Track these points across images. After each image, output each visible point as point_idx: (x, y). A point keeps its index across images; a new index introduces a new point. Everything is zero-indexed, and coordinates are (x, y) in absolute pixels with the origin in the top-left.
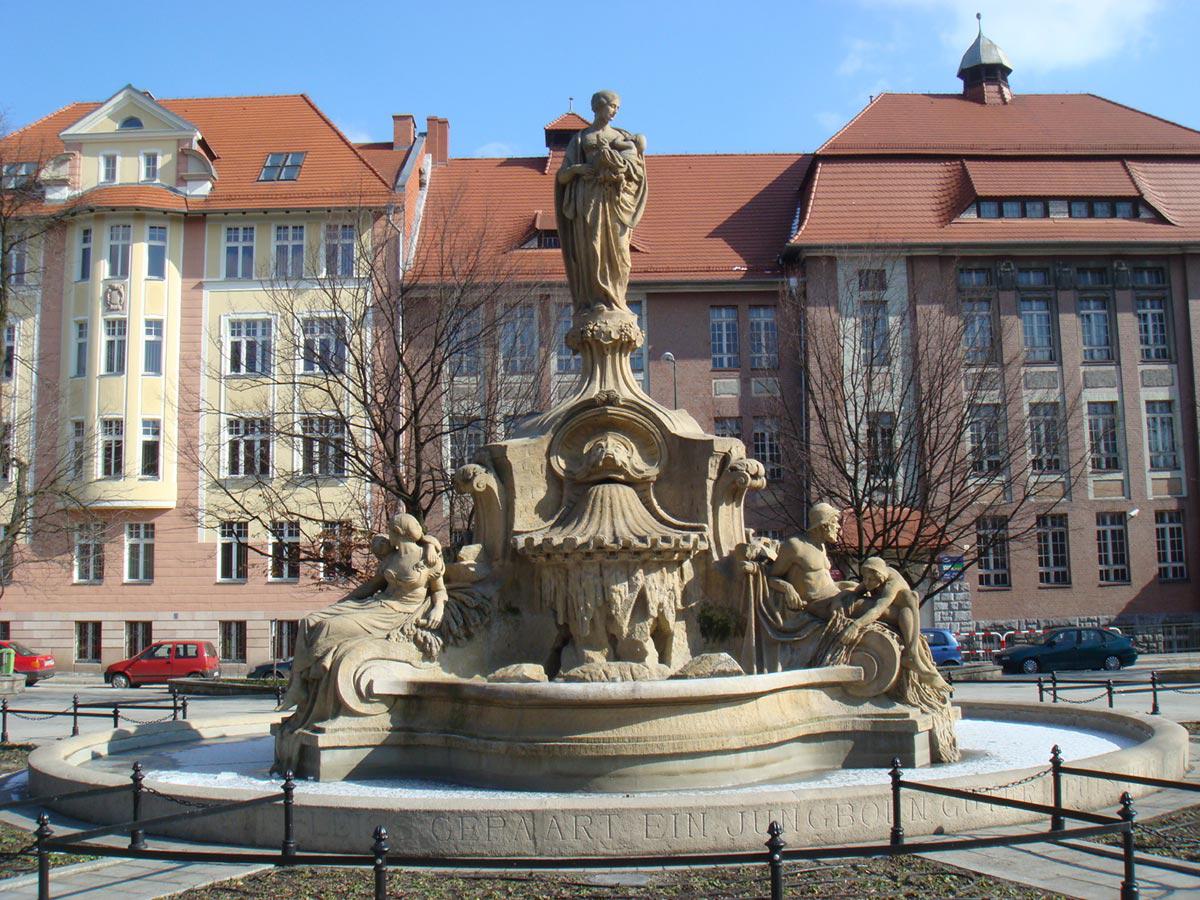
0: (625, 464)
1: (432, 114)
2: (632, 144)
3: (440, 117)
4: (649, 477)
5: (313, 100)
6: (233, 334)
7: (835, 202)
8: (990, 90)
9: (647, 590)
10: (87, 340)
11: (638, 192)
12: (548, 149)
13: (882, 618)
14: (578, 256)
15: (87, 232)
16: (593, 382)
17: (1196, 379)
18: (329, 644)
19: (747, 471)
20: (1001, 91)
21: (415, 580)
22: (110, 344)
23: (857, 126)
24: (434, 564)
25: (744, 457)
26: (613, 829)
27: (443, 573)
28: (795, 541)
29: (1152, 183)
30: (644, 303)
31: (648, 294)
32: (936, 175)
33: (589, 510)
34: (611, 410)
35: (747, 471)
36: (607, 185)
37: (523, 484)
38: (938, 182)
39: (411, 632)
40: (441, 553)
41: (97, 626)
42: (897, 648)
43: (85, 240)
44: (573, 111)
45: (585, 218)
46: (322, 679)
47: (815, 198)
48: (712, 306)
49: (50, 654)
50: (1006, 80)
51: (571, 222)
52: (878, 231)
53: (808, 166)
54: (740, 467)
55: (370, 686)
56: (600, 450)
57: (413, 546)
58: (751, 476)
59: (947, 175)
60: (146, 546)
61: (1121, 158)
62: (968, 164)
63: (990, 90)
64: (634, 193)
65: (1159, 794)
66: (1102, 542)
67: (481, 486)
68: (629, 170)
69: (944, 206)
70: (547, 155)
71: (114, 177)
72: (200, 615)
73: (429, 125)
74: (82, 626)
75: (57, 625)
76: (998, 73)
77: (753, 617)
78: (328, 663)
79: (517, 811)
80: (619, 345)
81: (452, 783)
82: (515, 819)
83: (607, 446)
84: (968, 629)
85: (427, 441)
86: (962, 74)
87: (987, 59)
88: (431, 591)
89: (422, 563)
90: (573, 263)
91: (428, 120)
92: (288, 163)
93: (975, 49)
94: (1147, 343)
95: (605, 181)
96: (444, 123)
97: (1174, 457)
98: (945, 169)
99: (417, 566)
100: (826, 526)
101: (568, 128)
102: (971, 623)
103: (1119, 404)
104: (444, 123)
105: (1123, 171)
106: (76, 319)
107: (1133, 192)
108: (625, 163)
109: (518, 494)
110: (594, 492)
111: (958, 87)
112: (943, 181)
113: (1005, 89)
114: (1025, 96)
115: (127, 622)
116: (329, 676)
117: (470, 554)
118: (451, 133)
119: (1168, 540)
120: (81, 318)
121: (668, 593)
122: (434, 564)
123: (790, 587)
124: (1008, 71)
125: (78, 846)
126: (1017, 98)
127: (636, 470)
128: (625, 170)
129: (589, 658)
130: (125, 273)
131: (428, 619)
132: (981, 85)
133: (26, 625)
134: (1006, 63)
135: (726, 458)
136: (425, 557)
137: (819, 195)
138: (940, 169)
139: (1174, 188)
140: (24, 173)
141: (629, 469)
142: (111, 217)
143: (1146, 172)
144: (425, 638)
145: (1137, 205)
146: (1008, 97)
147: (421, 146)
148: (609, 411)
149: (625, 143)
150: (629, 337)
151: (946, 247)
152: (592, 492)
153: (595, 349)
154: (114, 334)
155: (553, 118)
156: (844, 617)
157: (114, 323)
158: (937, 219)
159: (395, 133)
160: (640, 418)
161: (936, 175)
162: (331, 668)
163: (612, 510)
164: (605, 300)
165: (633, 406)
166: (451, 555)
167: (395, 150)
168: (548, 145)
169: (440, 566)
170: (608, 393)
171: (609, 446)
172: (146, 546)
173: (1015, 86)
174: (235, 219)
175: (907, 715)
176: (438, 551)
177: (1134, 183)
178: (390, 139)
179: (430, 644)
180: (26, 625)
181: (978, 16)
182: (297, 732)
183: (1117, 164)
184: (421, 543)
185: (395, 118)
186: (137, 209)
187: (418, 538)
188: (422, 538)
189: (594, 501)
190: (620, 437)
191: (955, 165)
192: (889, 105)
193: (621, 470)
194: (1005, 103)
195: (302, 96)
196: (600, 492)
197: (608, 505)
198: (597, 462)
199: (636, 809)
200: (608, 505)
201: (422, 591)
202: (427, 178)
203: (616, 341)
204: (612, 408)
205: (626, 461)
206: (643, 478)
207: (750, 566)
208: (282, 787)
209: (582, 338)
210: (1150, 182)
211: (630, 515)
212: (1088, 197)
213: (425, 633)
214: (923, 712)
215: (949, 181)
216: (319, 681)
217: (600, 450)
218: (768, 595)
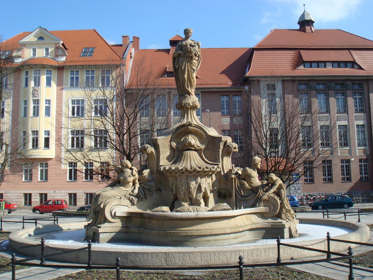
0: (194, 144)
1: (134, 36)
2: (197, 45)
3: (137, 36)
4: (202, 148)
5: (97, 31)
6: (72, 104)
7: (259, 63)
8: (308, 28)
9: (201, 184)
10: (27, 106)
11: (198, 60)
12: (170, 46)
13: (274, 192)
14: (180, 80)
15: (27, 72)
16: (184, 119)
17: (372, 118)
18: (102, 201)
19: (232, 147)
20: (311, 28)
21: (129, 180)
22: (34, 107)
23: (266, 39)
24: (135, 175)
25: (231, 142)
26: (190, 258)
27: (138, 178)
28: (247, 168)
29: (358, 57)
30: (200, 94)
31: (201, 91)
32: (291, 55)
33: (183, 159)
34: (190, 127)
35: (232, 147)
36: (189, 57)
37: (163, 150)
38: (292, 57)
39: (128, 197)
40: (137, 172)
41: (30, 195)
42: (279, 202)
43: (27, 75)
44: (178, 34)
45: (182, 68)
46: (100, 211)
47: (253, 62)
48: (221, 95)
49: (15, 203)
50: (313, 25)
51: (178, 69)
52: (273, 72)
53: (251, 52)
54: (230, 145)
55: (115, 213)
56: (187, 140)
57: (129, 170)
58: (233, 148)
59: (294, 54)
60: (45, 170)
61: (349, 49)
62: (301, 51)
63: (308, 28)
64: (197, 60)
65: (360, 247)
66: (343, 169)
67: (149, 151)
68: (195, 53)
69: (293, 64)
70: (170, 48)
71: (35, 55)
72: (62, 191)
73: (133, 39)
74: (26, 195)
75: (18, 194)
76: (310, 23)
77: (234, 192)
78: (102, 206)
79: (161, 252)
80: (192, 107)
81: (141, 244)
82: (160, 255)
83: (189, 139)
84: (301, 196)
85: (133, 137)
86: (299, 23)
87: (307, 18)
88: (134, 184)
89: (131, 175)
90: (178, 82)
91: (133, 37)
92: (90, 51)
93: (303, 15)
94: (356, 107)
95: (188, 56)
96: (138, 38)
97: (365, 142)
98: (294, 52)
99: (130, 176)
100: (257, 164)
101: (177, 40)
102: (302, 194)
103: (348, 126)
104: (138, 38)
105: (349, 53)
106: (24, 99)
107: (352, 60)
108: (194, 51)
109: (161, 154)
110: (185, 153)
111: (298, 27)
112: (293, 56)
113: (312, 28)
114: (319, 30)
115: (39, 194)
116: (102, 210)
117: (146, 172)
118: (140, 41)
119: (363, 168)
120: (25, 99)
121: (208, 185)
122: (135, 175)
123: (246, 182)
124: (313, 22)
125: (24, 263)
126: (316, 31)
127: (198, 146)
128: (194, 53)
129: (183, 205)
130: (39, 85)
131: (133, 193)
132: (305, 26)
133: (8, 195)
134: (313, 20)
135: (226, 143)
136: (132, 173)
137: (254, 61)
138: (292, 53)
139: (365, 58)
140: (7, 54)
141: (195, 146)
142: (34, 68)
143: (356, 54)
144: (132, 198)
145: (353, 64)
146: (313, 30)
147: (131, 45)
148: (189, 128)
149: (194, 45)
150: (196, 105)
151: (294, 77)
152: (184, 153)
153: (185, 108)
154: (35, 104)
155: (172, 37)
156: (262, 192)
157: (35, 100)
158: (291, 68)
159: (123, 41)
160: (199, 130)
161: (291, 55)
162: (103, 208)
163: (190, 159)
164: (188, 93)
165: (197, 126)
166: (140, 173)
167: (123, 47)
168: (170, 45)
169: (137, 176)
170: (189, 122)
171: (189, 139)
172: (45, 170)
173: (316, 27)
174: (73, 68)
175: (282, 222)
176: (136, 172)
177: (352, 57)
178: (121, 43)
179: (134, 200)
180: (8, 195)
181: (304, 5)
182: (92, 228)
183: (347, 51)
184: (131, 169)
185: (123, 37)
186: (43, 65)
187: (130, 167)
188: (131, 167)
189: (185, 156)
190: (193, 136)
191: (297, 51)
192: (276, 33)
193: (193, 146)
194: (312, 32)
195: (94, 30)
196: (186, 153)
197: (189, 157)
198: (186, 144)
199: (198, 252)
200: (189, 157)
201: (131, 184)
202: (133, 55)
203: (191, 106)
204: (190, 127)
205: (195, 143)
206: (200, 149)
207: (233, 176)
208: (88, 245)
209: (181, 105)
210: (358, 57)
211: (196, 160)
212: (338, 61)
213: (132, 197)
214: (287, 221)
215: (295, 56)
216: (99, 212)
217: (187, 140)
218: (239, 185)
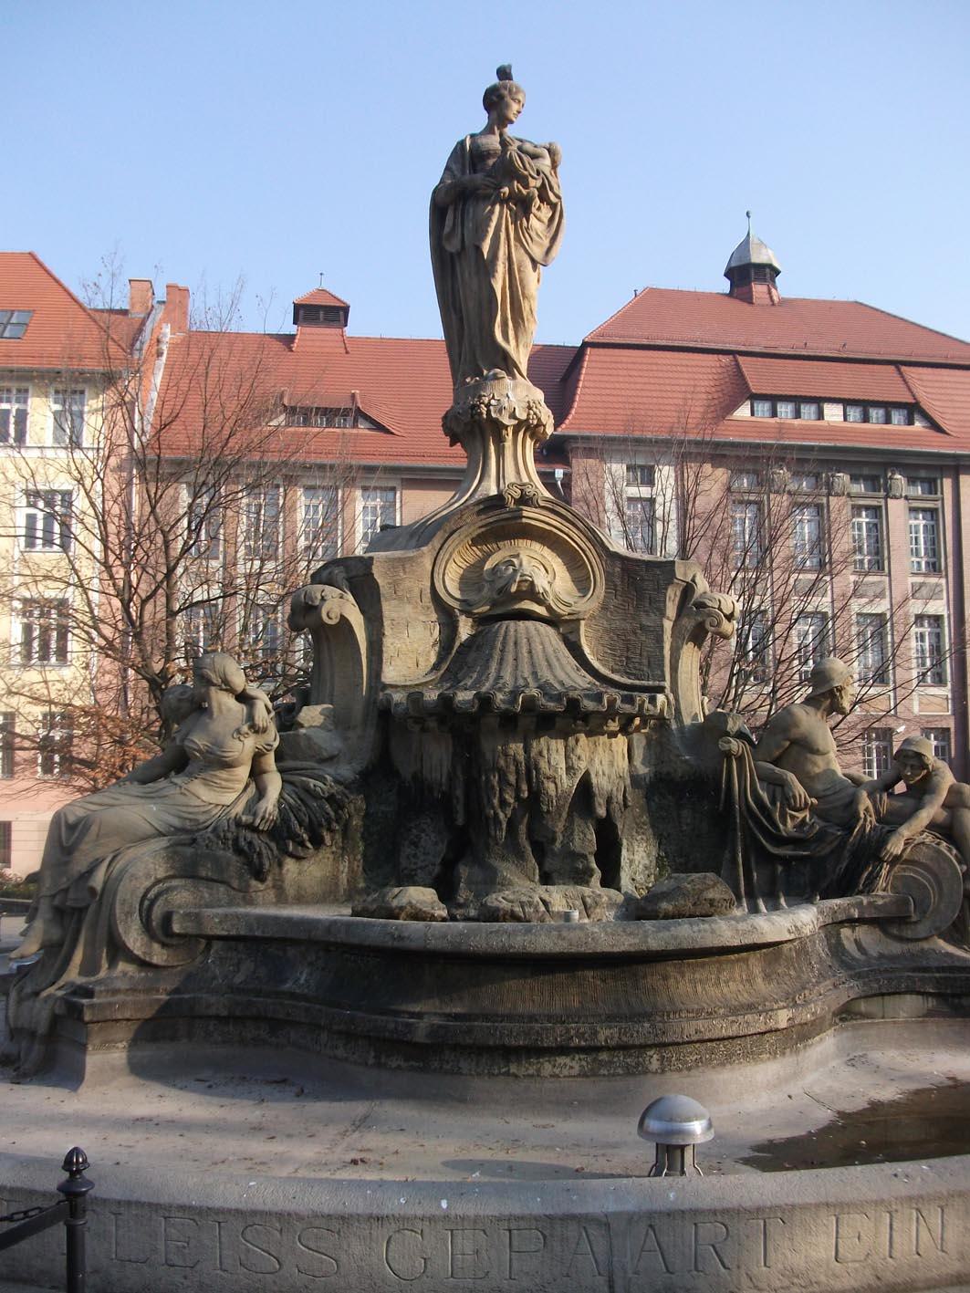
1: (171, 282)
3: (181, 285)
5: (41, 259)
7: (604, 392)
8: (758, 289)
9: (593, 776)
11: (551, 219)
13: (932, 826)
16: (486, 479)
17: (966, 595)
18: (98, 853)
20: (770, 293)
21: (236, 754)
23: (624, 317)
24: (265, 730)
27: (276, 744)
29: (929, 387)
32: (709, 370)
33: (496, 657)
35: (720, 609)
37: (394, 615)
39: (229, 835)
40: (273, 714)
44: (324, 287)
45: (478, 249)
46: (87, 908)
47: (584, 387)
50: (774, 282)
52: (695, 396)
53: (578, 354)
54: (710, 604)
55: (167, 918)
56: (511, 569)
57: (229, 701)
58: (725, 616)
61: (897, 364)
62: (740, 359)
63: (758, 289)
64: (546, 221)
67: (332, 615)
69: (716, 402)
76: (768, 273)
78: (98, 880)
83: (521, 565)
85: (180, 610)
86: (729, 274)
87: (758, 257)
88: (256, 773)
89: (245, 728)
91: (167, 287)
92: (14, 320)
93: (745, 245)
94: (917, 555)
99: (238, 731)
100: (840, 689)
105: (896, 375)
107: (909, 399)
109: (387, 631)
110: (503, 632)
111: (725, 286)
113: (773, 290)
114: (795, 300)
116: (100, 903)
117: (312, 716)
121: (616, 782)
122: (265, 730)
123: (791, 777)
124: (777, 272)
126: (783, 302)
127: (559, 600)
129: (505, 878)
131: (255, 815)
132: (750, 283)
134: (776, 264)
135: (688, 589)
136: (250, 718)
137: (587, 384)
139: (948, 398)
141: (551, 600)
143: (921, 380)
144: (250, 843)
145: (913, 410)
146: (775, 298)
147: (159, 313)
148: (525, 514)
150: (539, 419)
152: (497, 632)
155: (302, 292)
161: (709, 370)
162: (104, 889)
163: (532, 657)
166: (286, 719)
169: (273, 737)
171: (524, 563)
173: (786, 287)
176: (269, 712)
177: (909, 389)
179: (260, 854)
181: (748, 214)
182: (44, 994)
183: (893, 367)
184: (243, 698)
187: (240, 689)
188: (244, 690)
189: (504, 643)
191: (726, 359)
192: (653, 301)
194: (773, 304)
196: (512, 632)
197: (525, 650)
198: (508, 585)
200: (525, 650)
201: (243, 772)
202: (165, 348)
204: (528, 509)
205: (548, 588)
207: (735, 746)
209: (472, 416)
210: (927, 386)
211: (557, 664)
212: (864, 401)
213: (249, 835)
216: (81, 911)
217: (511, 568)
